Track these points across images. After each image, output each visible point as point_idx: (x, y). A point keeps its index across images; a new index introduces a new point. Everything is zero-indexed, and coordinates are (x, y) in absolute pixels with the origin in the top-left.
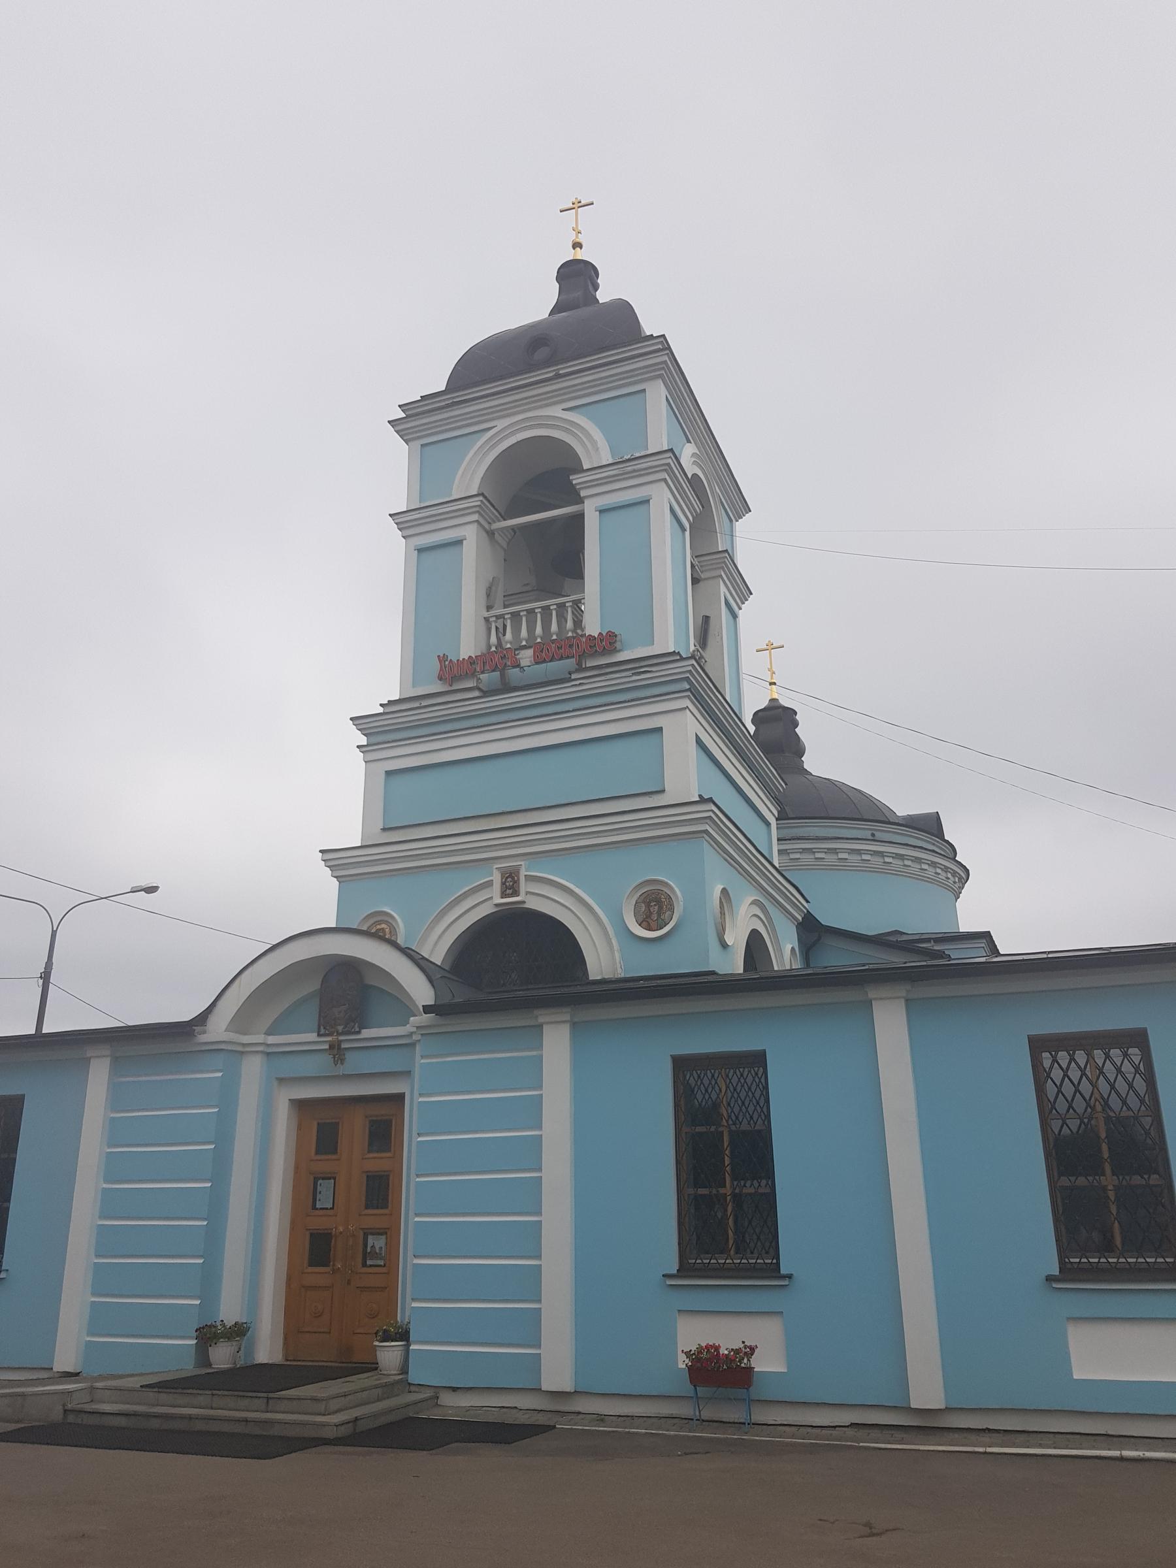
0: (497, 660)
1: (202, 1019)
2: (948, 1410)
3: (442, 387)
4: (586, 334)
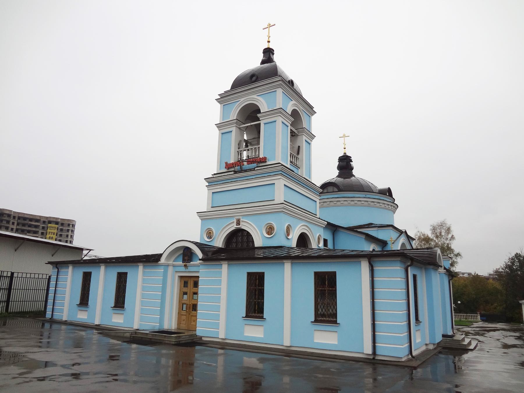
0: (240, 162)
2: (291, 346)
3: (229, 88)
4: (266, 74)
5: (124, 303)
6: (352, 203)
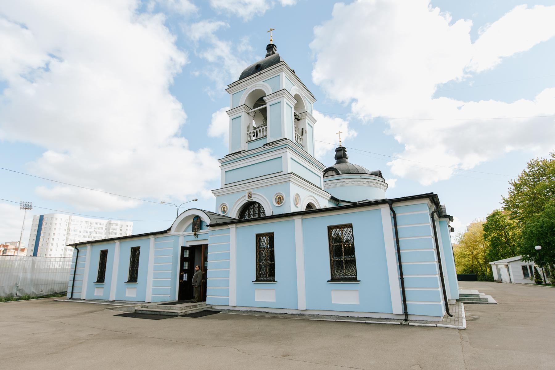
1: (170, 229)
5: (137, 278)
6: (350, 183)
